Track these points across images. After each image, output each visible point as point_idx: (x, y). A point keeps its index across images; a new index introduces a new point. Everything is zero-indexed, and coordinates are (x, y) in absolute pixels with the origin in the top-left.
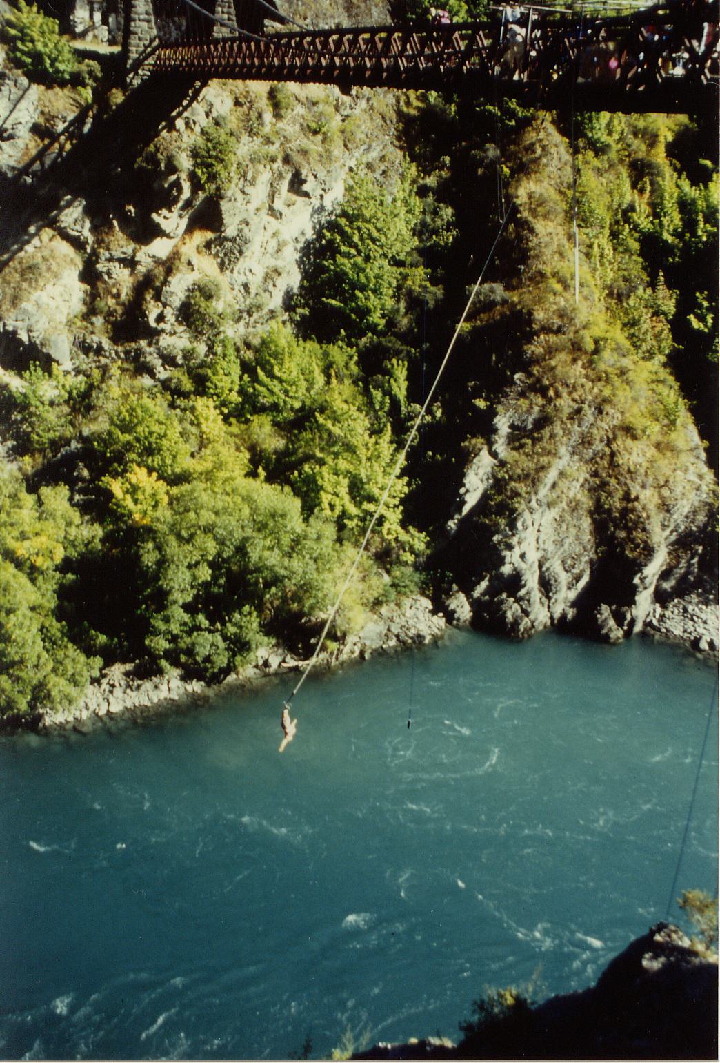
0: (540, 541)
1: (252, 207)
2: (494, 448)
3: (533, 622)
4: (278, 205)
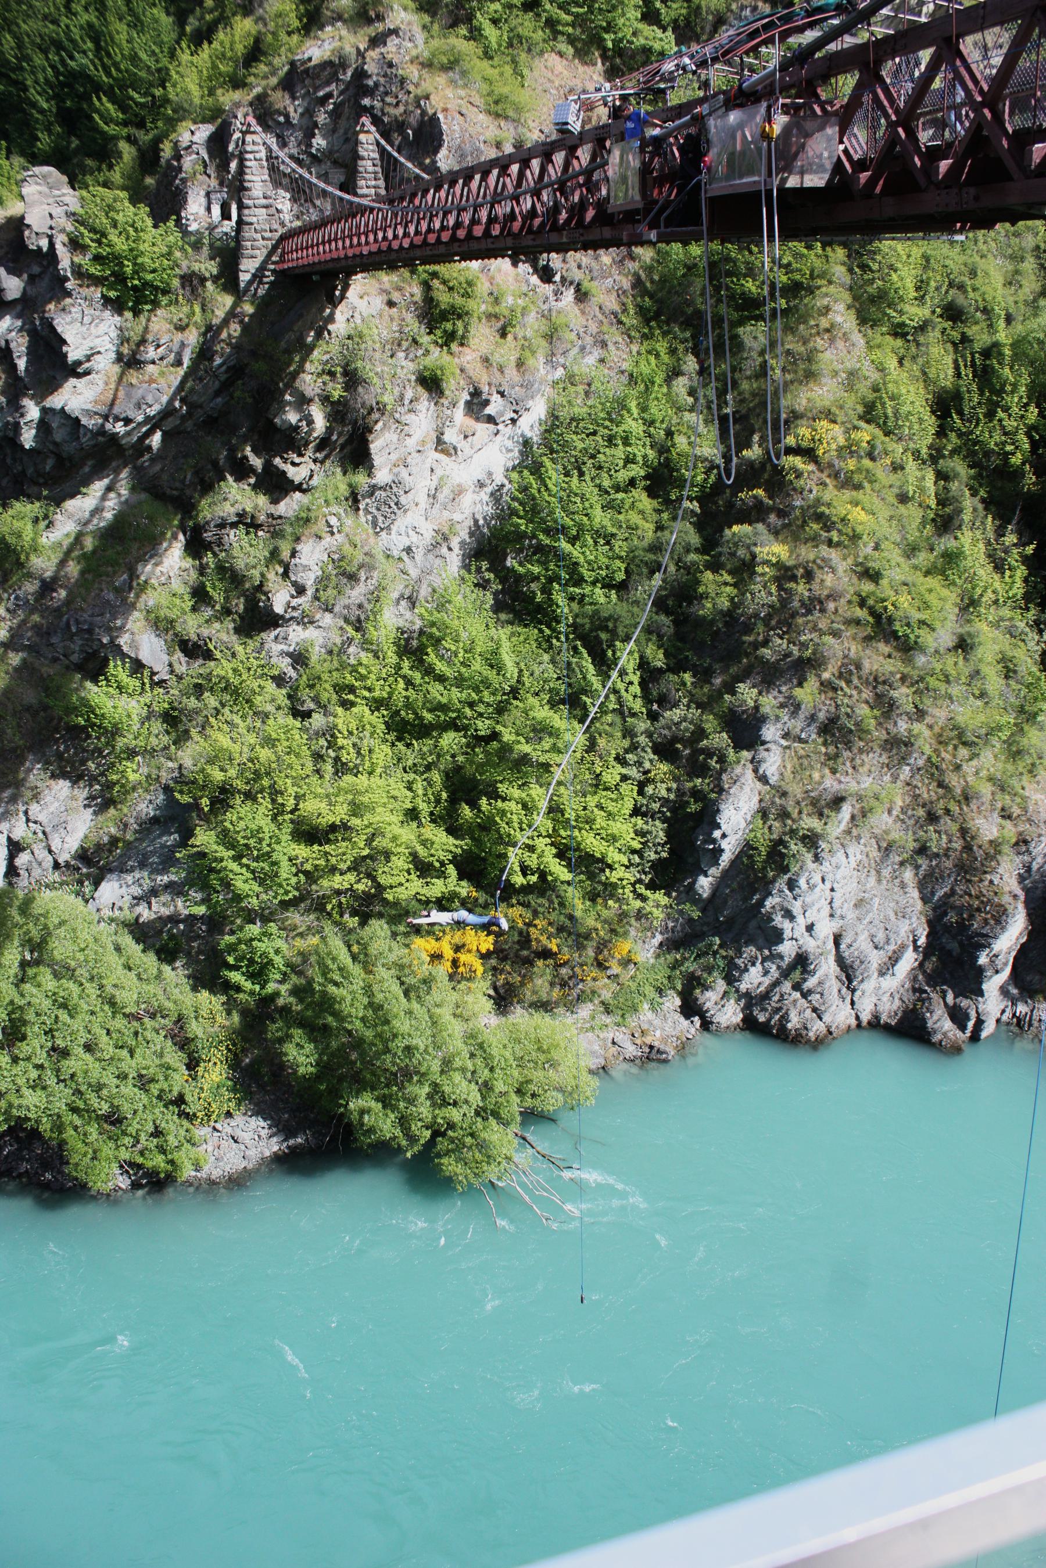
0: (835, 905)
1: (411, 443)
2: (761, 771)
3: (828, 1028)
4: (451, 436)
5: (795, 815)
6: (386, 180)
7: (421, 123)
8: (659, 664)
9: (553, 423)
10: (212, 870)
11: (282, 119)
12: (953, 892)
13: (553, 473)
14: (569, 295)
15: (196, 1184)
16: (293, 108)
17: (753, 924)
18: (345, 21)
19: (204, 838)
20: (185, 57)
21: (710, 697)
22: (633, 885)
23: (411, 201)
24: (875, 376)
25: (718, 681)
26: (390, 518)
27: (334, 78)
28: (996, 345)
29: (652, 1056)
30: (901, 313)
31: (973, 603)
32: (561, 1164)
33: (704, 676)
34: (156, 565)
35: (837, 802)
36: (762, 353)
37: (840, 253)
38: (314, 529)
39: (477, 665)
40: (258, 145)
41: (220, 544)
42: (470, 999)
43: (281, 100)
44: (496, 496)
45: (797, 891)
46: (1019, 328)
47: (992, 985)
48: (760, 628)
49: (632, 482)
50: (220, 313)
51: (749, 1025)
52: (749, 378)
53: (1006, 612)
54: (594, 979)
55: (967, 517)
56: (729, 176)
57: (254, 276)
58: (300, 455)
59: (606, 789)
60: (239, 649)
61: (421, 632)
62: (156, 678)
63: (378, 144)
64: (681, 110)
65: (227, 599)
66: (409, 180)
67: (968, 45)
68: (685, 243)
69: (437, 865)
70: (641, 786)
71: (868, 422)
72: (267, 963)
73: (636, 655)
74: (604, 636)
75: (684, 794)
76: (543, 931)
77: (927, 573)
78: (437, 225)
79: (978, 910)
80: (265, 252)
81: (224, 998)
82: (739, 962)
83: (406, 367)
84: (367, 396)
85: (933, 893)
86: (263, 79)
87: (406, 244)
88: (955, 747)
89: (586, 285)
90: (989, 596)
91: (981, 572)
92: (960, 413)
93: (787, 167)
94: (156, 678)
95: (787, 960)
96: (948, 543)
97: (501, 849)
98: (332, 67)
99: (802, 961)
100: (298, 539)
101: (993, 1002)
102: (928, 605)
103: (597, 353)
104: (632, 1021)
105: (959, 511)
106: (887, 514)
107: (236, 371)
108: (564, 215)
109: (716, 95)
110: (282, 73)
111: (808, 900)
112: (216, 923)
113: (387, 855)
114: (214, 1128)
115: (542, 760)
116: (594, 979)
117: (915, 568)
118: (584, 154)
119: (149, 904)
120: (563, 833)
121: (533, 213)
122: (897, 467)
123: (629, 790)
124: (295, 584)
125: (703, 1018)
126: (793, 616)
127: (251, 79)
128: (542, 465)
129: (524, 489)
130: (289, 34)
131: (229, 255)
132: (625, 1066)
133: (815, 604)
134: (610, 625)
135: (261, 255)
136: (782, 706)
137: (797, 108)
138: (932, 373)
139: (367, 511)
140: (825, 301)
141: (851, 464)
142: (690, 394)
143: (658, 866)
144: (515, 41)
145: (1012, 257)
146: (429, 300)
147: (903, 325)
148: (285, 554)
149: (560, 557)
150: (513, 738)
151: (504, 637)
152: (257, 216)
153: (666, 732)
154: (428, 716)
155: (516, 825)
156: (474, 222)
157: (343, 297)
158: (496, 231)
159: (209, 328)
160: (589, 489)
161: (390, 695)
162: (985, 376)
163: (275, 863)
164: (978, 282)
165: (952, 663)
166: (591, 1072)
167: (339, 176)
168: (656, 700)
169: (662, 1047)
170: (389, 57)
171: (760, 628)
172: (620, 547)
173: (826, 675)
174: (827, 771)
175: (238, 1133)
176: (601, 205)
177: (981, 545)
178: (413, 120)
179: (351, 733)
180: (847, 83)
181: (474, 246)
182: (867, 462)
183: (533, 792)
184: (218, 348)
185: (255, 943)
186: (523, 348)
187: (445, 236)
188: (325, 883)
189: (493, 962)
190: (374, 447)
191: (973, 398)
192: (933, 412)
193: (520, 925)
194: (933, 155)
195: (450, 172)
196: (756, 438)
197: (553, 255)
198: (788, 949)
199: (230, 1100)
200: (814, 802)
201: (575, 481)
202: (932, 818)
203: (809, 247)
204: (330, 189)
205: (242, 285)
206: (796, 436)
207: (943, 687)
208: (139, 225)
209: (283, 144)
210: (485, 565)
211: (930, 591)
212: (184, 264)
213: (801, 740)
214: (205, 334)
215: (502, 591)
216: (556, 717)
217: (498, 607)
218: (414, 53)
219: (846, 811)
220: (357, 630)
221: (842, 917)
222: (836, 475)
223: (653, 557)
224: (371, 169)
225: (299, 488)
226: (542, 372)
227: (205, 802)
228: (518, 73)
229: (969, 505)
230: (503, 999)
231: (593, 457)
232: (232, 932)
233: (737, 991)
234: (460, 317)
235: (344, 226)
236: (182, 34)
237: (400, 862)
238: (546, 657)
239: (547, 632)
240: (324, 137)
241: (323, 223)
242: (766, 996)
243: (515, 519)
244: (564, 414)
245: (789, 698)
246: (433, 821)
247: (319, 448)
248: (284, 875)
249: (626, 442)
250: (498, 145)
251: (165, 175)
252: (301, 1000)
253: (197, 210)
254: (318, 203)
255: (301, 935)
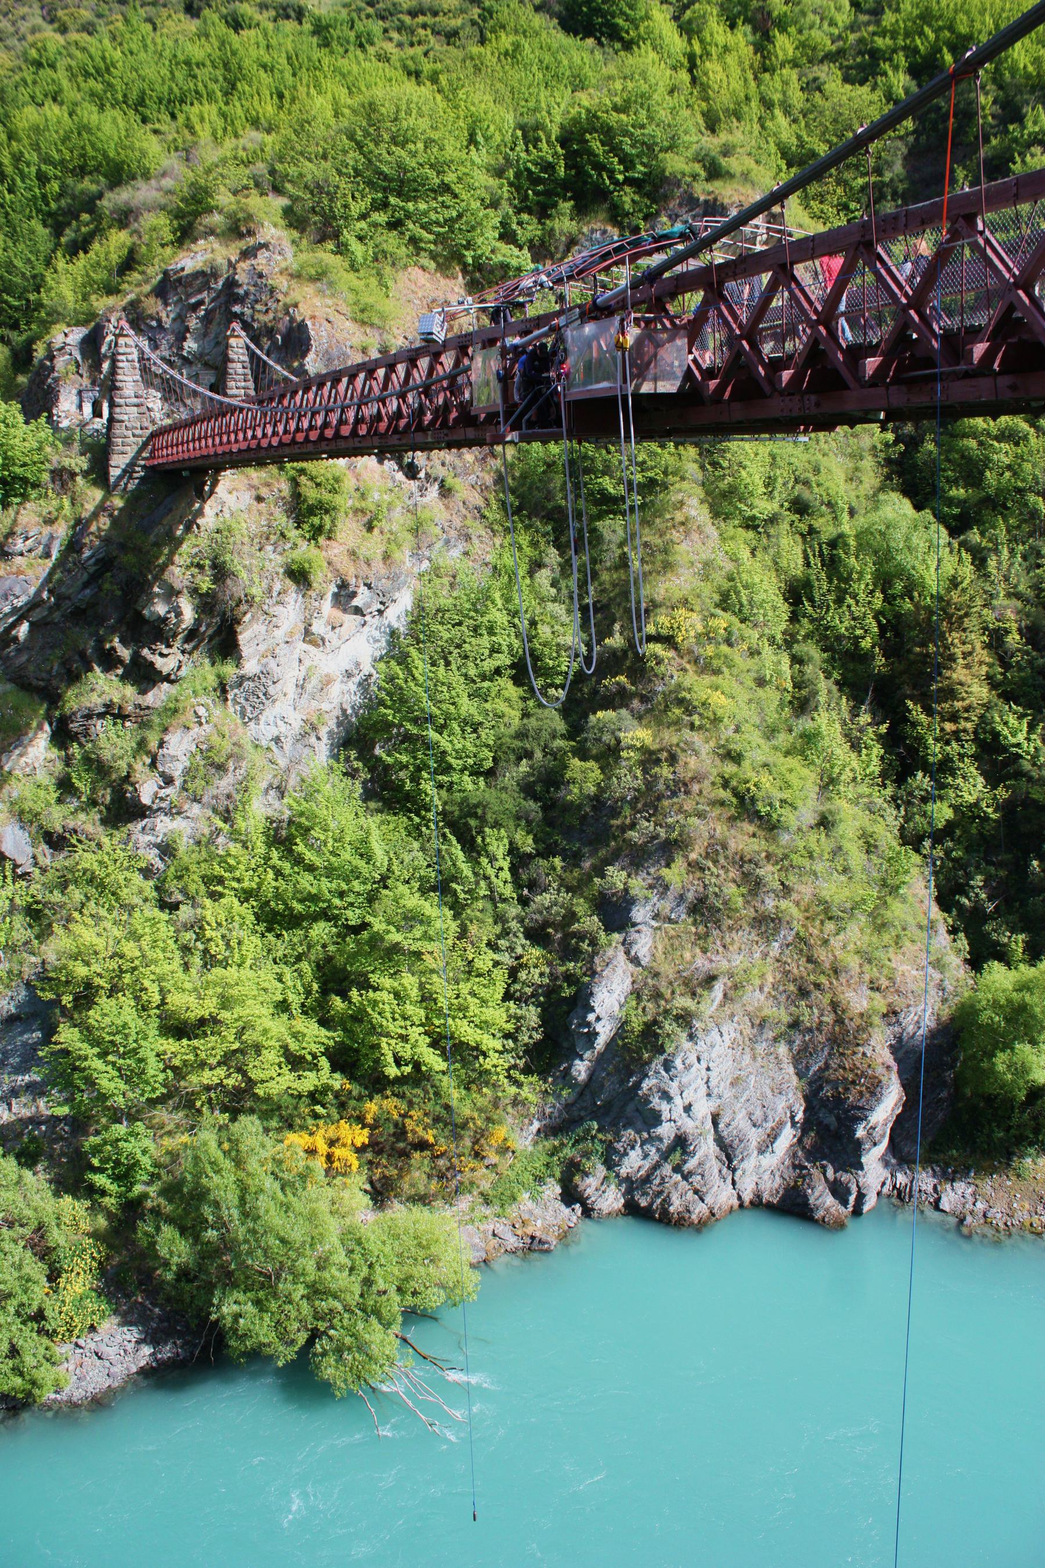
1: (279, 634)
4: (319, 627)
5: (668, 996)
6: (256, 381)
7: (290, 330)
8: (528, 850)
9: (419, 615)
10: (75, 1069)
11: (154, 323)
12: (827, 1066)
13: (420, 664)
14: (434, 491)
15: (55, 1407)
16: (167, 315)
17: (630, 1108)
18: (217, 236)
19: (68, 1035)
20: (61, 264)
21: (580, 881)
22: (508, 1070)
23: (280, 402)
24: (729, 566)
25: (587, 864)
26: (258, 710)
27: (206, 286)
28: (841, 536)
29: (534, 1246)
30: (751, 507)
31: (833, 781)
32: (444, 1365)
33: (573, 859)
34: (21, 755)
35: (710, 979)
36: (621, 545)
37: (692, 451)
38: (182, 719)
39: (347, 855)
40: (131, 346)
41: (86, 734)
42: (346, 1194)
43: (153, 306)
44: (364, 685)
45: (673, 1072)
46: (861, 521)
47: (873, 1158)
48: (627, 811)
49: (498, 671)
50: (90, 507)
51: (632, 1209)
52: (609, 569)
53: (864, 789)
54: (472, 1170)
55: (822, 698)
56: (585, 384)
57: (125, 471)
58: (169, 646)
59: (479, 975)
60: (105, 840)
61: (291, 822)
62: (19, 871)
63: (248, 348)
64: (539, 321)
65: (93, 790)
66: (277, 382)
67: (800, 270)
68: (544, 443)
69: (309, 1058)
70: (513, 973)
71: (724, 610)
72: (134, 1165)
73: (506, 841)
74: (473, 823)
75: (557, 978)
76: (419, 1122)
77: (787, 753)
78: (306, 424)
79: (853, 1082)
80: (135, 448)
81: (88, 1203)
82: (619, 1146)
83: (274, 560)
84: (234, 589)
85: (808, 1068)
86: (137, 286)
87: (275, 442)
88: (822, 923)
89: (450, 481)
90: (847, 776)
91: (838, 751)
92: (811, 600)
93: (641, 374)
94: (19, 871)
95: (666, 1142)
96: (804, 724)
97: (374, 1039)
98: (204, 277)
99: (681, 1142)
100: (166, 730)
101: (874, 1171)
102: (789, 785)
103: (461, 546)
104: (512, 1211)
105: (815, 693)
106: (747, 697)
107: (105, 564)
108: (429, 416)
109: (571, 309)
110: (155, 281)
111: (685, 1080)
112: (79, 1124)
113: (258, 1048)
114: (77, 1345)
115: (413, 948)
116: (472, 1170)
117: (776, 748)
118: (448, 360)
119: (9, 1105)
120: (437, 1022)
121: (399, 414)
122: (754, 653)
123: (500, 976)
124: (162, 775)
125: (584, 1204)
126: (659, 798)
127: (125, 286)
128: (408, 655)
129: (391, 679)
130: (163, 246)
131: (100, 453)
132: (506, 1258)
133: (680, 787)
134: (479, 811)
135: (131, 451)
136: (651, 887)
137: (648, 322)
138: (784, 563)
139: (235, 702)
140: (680, 497)
141: (710, 650)
142: (552, 585)
143: (531, 1051)
144: (380, 256)
145: (852, 456)
146: (297, 496)
147: (753, 518)
148: (153, 745)
149: (428, 745)
150: (383, 926)
151: (373, 826)
152: (128, 415)
153: (537, 917)
154: (298, 907)
155: (388, 1015)
156: (341, 422)
157: (212, 492)
158: (363, 430)
159: (78, 521)
160: (456, 679)
161: (260, 885)
162: (832, 564)
163: (141, 1060)
164: (822, 478)
165: (816, 840)
166: (473, 1266)
167: (210, 377)
168: (527, 886)
169: (544, 1238)
170: (259, 268)
171: (627, 811)
172: (487, 735)
173: (693, 856)
174: (698, 950)
175: (103, 1349)
176: (465, 408)
177: (838, 726)
178: (282, 326)
179: (219, 925)
180: (694, 299)
181: (342, 445)
182: (724, 648)
183: (405, 981)
184: (86, 540)
185: (121, 1144)
186: (389, 541)
187: (314, 436)
188: (193, 1078)
189: (369, 1156)
190: (243, 638)
191: (822, 585)
192: (786, 600)
193: (396, 1117)
194: (776, 366)
195: (318, 375)
196: (617, 627)
197: (419, 453)
198: (666, 1131)
199: (93, 1313)
200: (686, 982)
201: (442, 669)
202: (803, 993)
203: (663, 446)
204: (200, 389)
205: (112, 480)
206: (656, 624)
207: (806, 863)
208: (10, 421)
209: (155, 346)
210: (353, 754)
211: (791, 771)
212: (55, 459)
213: (670, 921)
214: (74, 527)
215: (371, 780)
216: (427, 904)
217: (368, 795)
218: (284, 265)
219: (719, 989)
220: (226, 820)
221: (720, 1097)
222: (696, 661)
223: (519, 744)
224: (240, 371)
225: (167, 679)
226: (408, 564)
227: (67, 1000)
228: (382, 285)
229: (824, 687)
230: (380, 1193)
231: (459, 646)
232: (97, 1133)
233: (618, 1176)
234: (327, 512)
235: (215, 425)
236: (58, 244)
237: (271, 1056)
238: (416, 845)
239: (417, 820)
240: (196, 340)
241: (193, 422)
242: (647, 1180)
243: (383, 710)
244: (430, 605)
245: (659, 878)
246: (304, 1013)
247: (187, 640)
248: (151, 1072)
249: (491, 631)
250: (364, 350)
251: (38, 374)
252: (170, 1201)
253: (70, 407)
254: (188, 402)
255: (169, 1133)
